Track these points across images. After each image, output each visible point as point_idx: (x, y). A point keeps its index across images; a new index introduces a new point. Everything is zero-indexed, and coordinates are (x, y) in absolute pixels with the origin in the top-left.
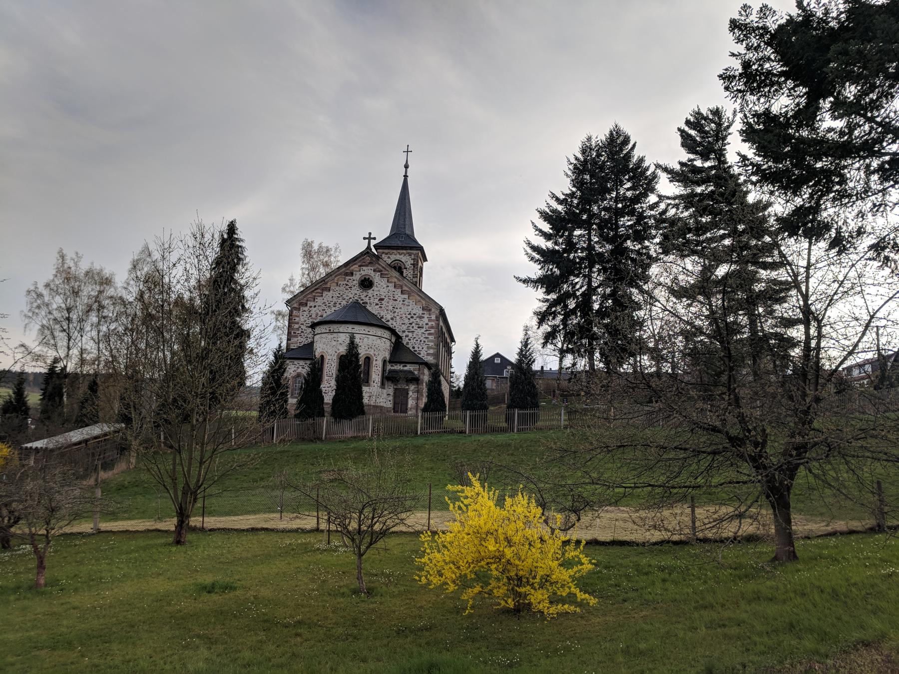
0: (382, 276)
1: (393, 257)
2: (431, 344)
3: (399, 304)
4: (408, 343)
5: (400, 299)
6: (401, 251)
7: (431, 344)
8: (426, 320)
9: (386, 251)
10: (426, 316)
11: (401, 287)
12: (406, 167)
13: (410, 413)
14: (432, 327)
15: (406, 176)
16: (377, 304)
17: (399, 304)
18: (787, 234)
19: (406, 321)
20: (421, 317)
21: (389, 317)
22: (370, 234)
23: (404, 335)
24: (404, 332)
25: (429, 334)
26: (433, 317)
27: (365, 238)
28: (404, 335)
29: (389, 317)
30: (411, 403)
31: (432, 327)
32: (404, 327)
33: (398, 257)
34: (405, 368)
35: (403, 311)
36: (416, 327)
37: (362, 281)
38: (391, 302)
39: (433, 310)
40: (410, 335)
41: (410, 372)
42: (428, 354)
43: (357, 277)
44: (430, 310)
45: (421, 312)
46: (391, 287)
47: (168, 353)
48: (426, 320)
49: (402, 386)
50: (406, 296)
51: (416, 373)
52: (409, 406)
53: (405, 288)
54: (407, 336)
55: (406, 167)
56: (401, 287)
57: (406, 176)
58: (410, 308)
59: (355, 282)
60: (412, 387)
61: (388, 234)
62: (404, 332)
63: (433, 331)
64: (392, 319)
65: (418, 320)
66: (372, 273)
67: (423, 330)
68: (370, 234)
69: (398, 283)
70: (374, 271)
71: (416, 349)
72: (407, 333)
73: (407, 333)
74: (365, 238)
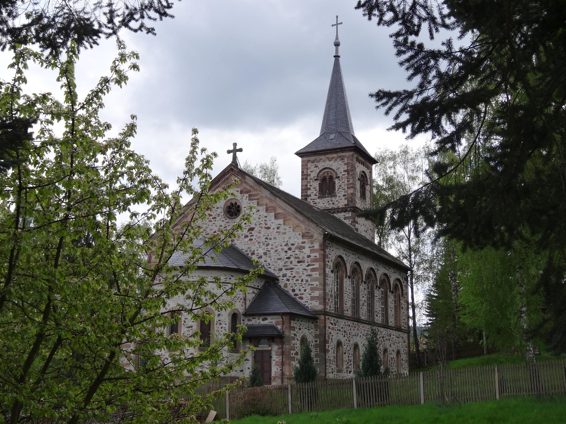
0: (251, 198)
1: (321, 165)
2: (316, 283)
3: (272, 233)
4: (286, 286)
5: (274, 226)
6: (330, 156)
7: (316, 283)
8: (307, 251)
9: (312, 158)
10: (307, 245)
11: (274, 209)
12: (337, 45)
13: (274, 384)
14: (315, 260)
15: (337, 57)
16: (246, 236)
17: (272, 233)
18: (505, 126)
19: (283, 255)
20: (301, 248)
21: (261, 252)
22: (235, 145)
23: (281, 274)
24: (281, 270)
25: (313, 270)
26: (317, 246)
27: (229, 152)
28: (281, 274)
29: (261, 252)
30: (275, 370)
31: (315, 260)
32: (281, 264)
33: (328, 164)
34: (266, 322)
35: (279, 241)
36: (295, 262)
37: (229, 208)
38: (264, 231)
39: (316, 236)
40: (288, 273)
41: (272, 327)
42: (312, 298)
43: (222, 203)
44: (312, 237)
45: (301, 240)
46: (263, 213)
47: (413, 260)
48: (307, 251)
49: (263, 347)
50: (281, 221)
51: (279, 327)
52: (273, 374)
53: (279, 211)
54: (284, 276)
55: (337, 45)
56: (274, 209)
57: (337, 57)
58: (286, 237)
59: (219, 210)
60: (275, 348)
61: (318, 136)
62: (281, 270)
63: (317, 265)
64: (265, 254)
65: (297, 252)
66: (238, 196)
67: (304, 265)
68: (235, 145)
69: (270, 204)
70: (241, 192)
71: (297, 292)
72: (284, 271)
73: (284, 271)
74: (229, 152)
